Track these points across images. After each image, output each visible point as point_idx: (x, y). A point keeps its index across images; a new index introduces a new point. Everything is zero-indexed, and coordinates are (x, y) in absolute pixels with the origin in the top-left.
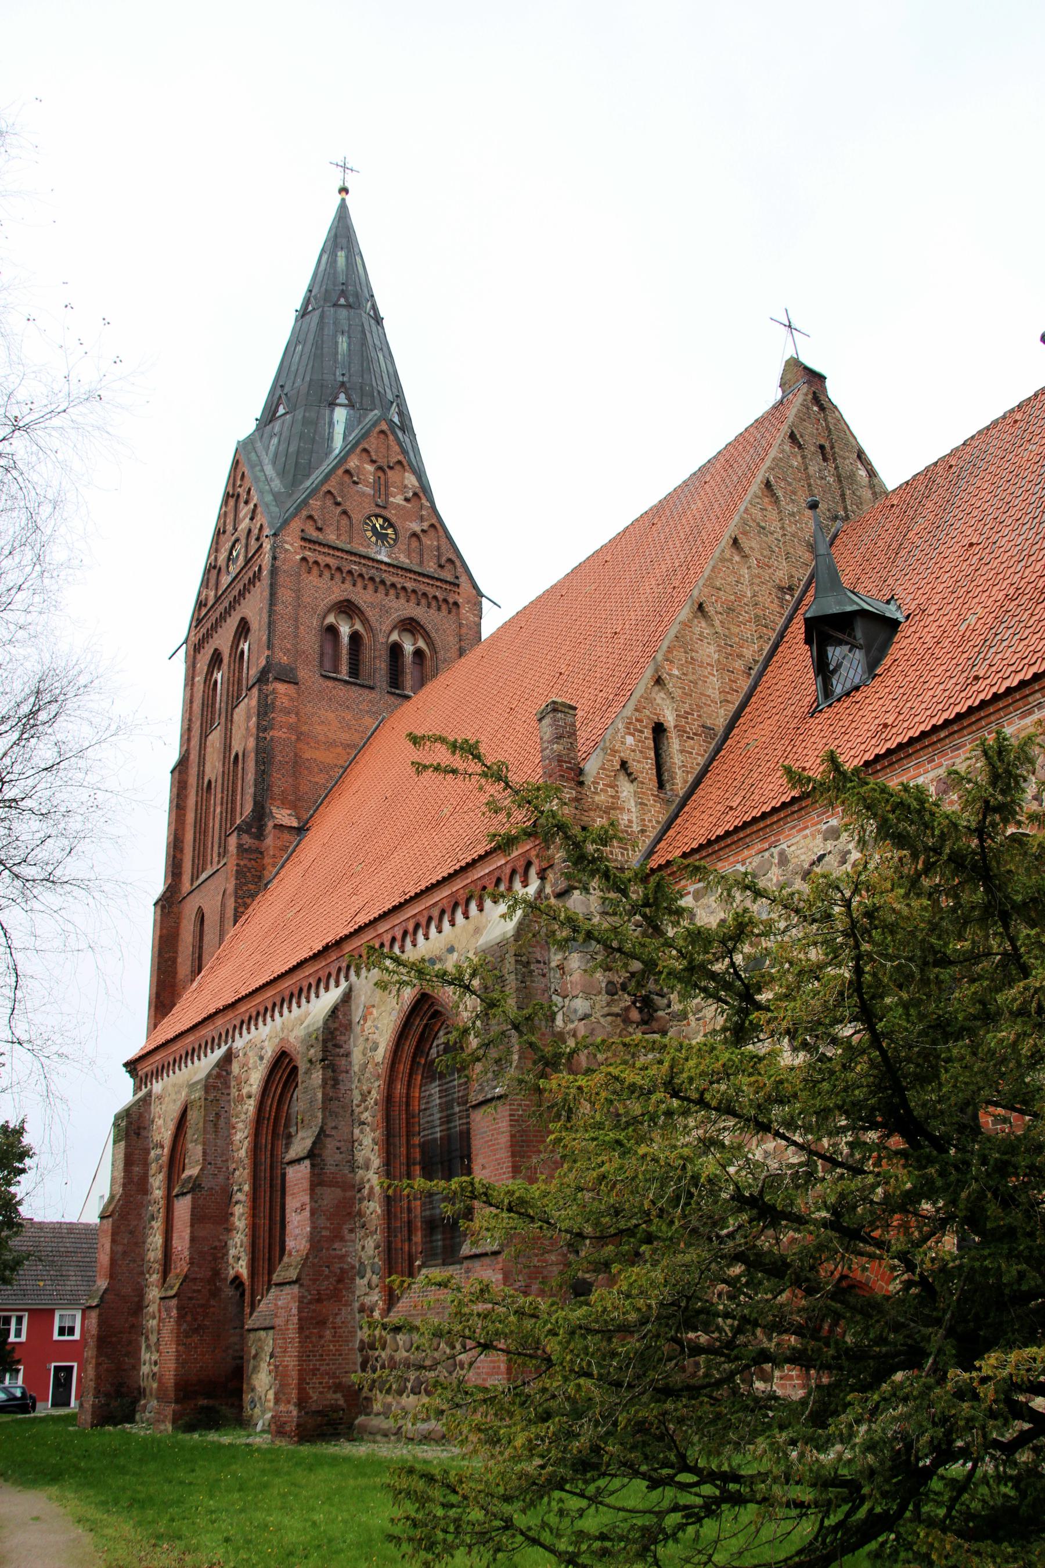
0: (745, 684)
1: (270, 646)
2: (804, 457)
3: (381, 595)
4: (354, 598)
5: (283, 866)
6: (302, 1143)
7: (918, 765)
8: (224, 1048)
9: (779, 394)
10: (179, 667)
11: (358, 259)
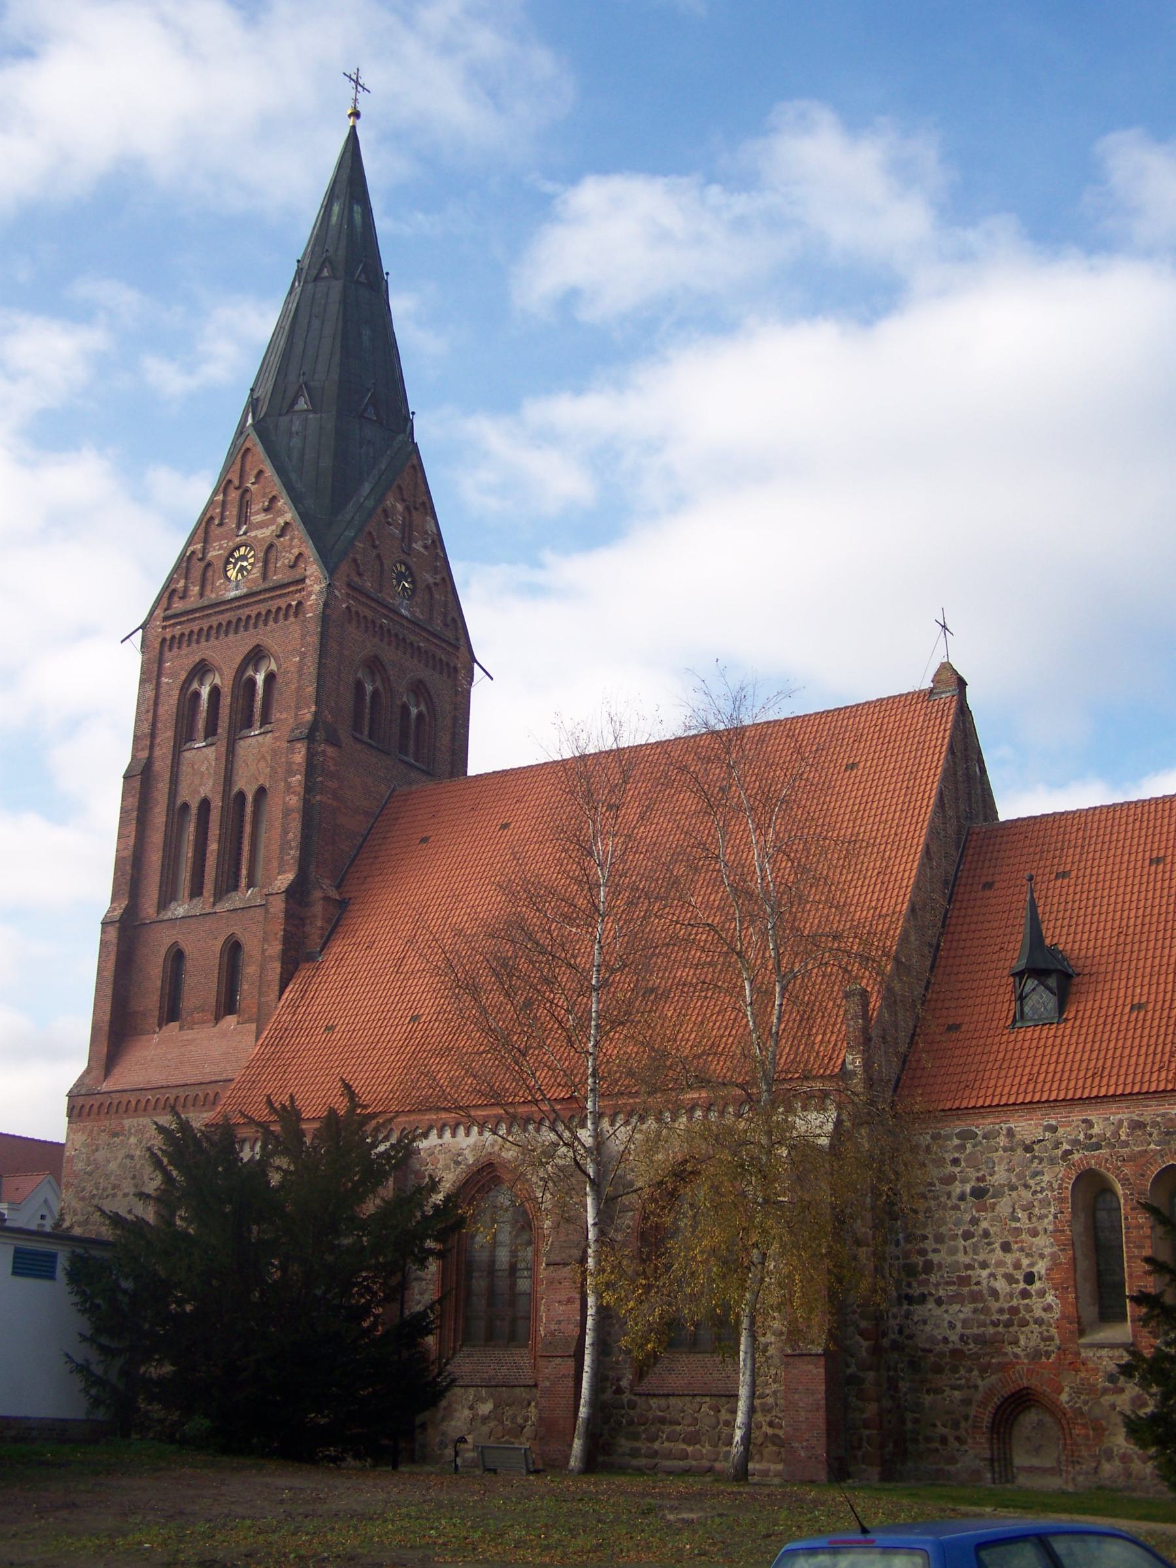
7: (1119, 1108)
9: (927, 684)
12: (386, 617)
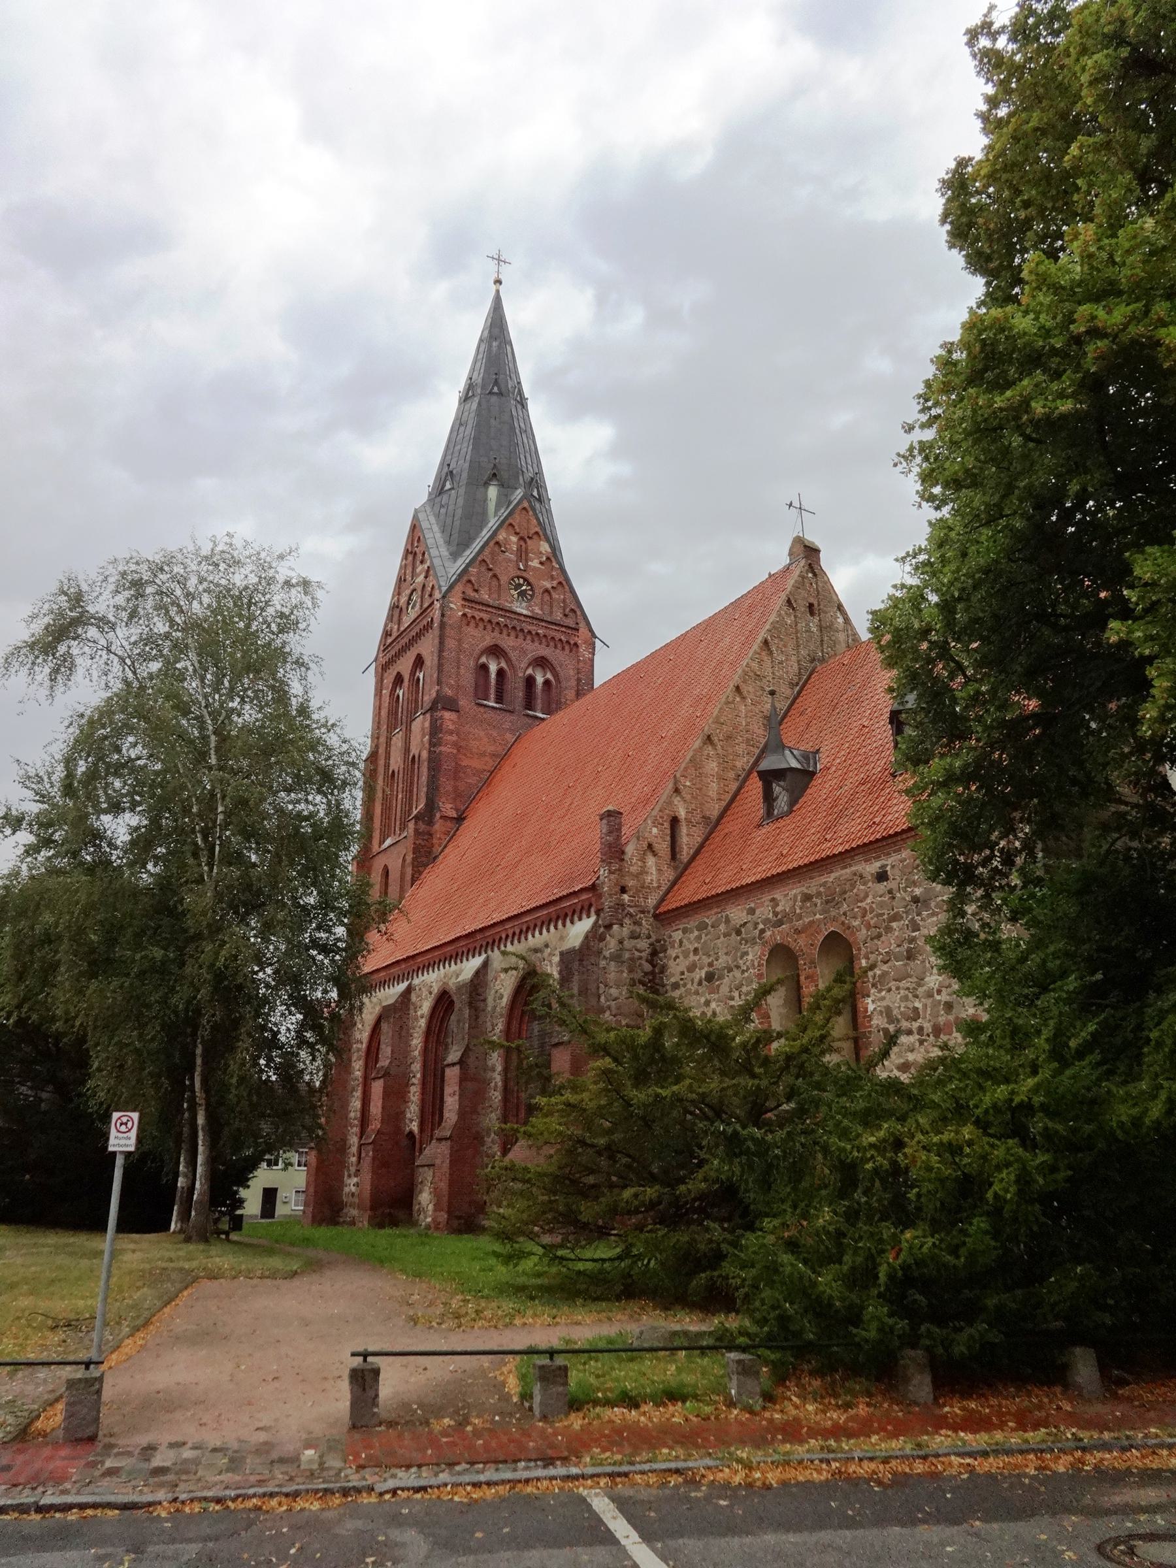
0: (734, 786)
1: (439, 683)
2: (795, 617)
3: (520, 640)
4: (500, 643)
5: (445, 847)
6: (454, 1055)
8: (406, 984)
10: (370, 679)
11: (509, 348)
12: (502, 616)
